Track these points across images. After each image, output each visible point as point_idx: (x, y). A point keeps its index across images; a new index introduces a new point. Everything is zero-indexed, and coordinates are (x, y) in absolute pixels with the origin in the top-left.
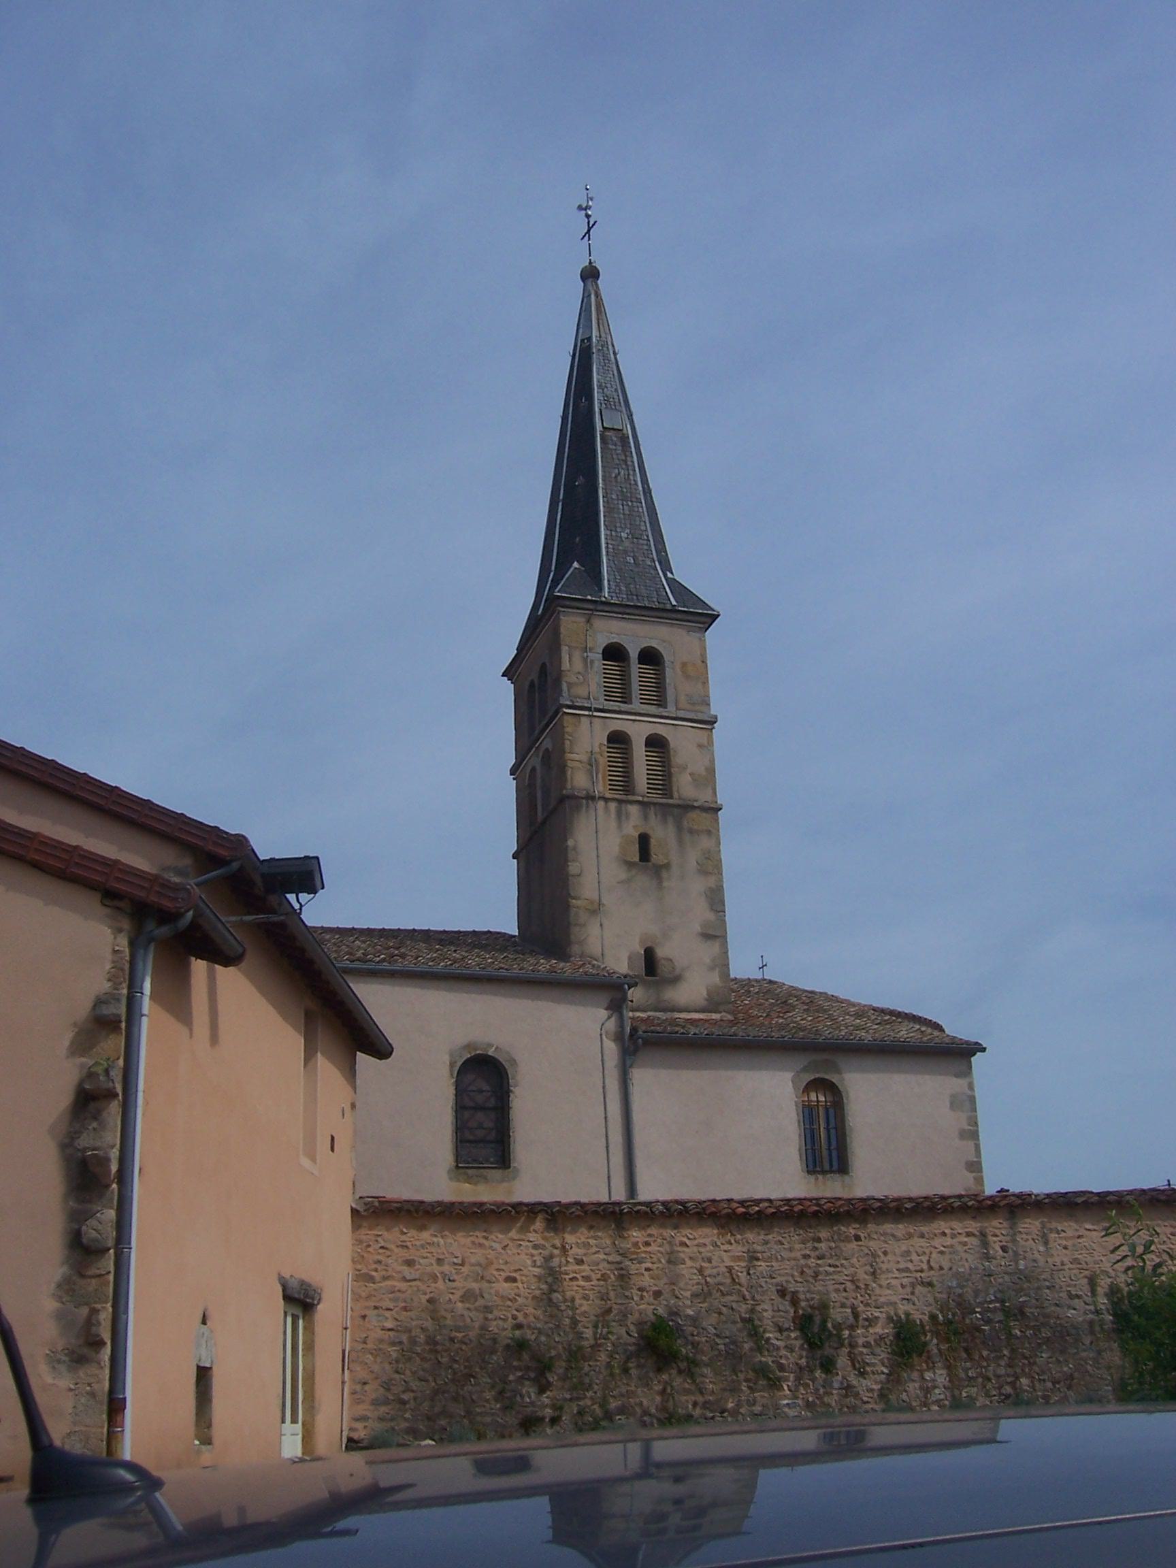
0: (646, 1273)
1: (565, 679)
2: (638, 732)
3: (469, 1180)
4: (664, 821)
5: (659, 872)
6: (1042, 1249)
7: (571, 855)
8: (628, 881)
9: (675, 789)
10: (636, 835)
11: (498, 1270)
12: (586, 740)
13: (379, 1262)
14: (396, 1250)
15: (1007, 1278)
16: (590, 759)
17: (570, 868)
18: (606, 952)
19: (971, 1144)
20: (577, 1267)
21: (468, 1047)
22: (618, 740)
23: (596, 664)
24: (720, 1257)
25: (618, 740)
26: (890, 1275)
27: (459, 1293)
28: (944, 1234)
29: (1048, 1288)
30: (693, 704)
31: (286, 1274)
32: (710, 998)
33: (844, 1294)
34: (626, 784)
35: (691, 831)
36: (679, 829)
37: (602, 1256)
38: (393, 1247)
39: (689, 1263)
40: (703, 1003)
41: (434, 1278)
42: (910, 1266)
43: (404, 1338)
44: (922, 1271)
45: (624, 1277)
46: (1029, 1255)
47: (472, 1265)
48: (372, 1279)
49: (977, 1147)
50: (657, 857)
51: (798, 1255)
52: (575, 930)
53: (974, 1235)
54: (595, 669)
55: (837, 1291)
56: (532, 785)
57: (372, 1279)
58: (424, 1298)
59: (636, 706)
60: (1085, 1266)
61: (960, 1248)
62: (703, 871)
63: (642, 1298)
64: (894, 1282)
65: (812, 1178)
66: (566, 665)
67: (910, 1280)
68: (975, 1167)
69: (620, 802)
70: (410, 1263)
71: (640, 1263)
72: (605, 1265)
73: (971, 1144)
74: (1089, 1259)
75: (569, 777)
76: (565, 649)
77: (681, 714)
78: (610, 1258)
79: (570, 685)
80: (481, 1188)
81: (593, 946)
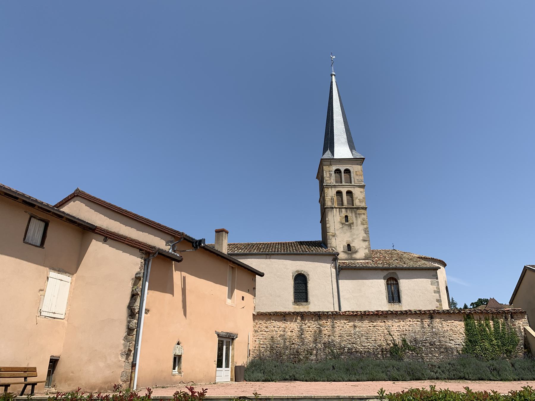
2: (344, 190)
3: (297, 305)
4: (352, 212)
5: (350, 225)
7: (327, 222)
8: (342, 227)
12: (331, 193)
15: (429, 334)
21: (297, 271)
22: (339, 193)
25: (339, 193)
28: (410, 321)
31: (220, 331)
32: (365, 257)
35: (359, 214)
36: (356, 214)
41: (273, 331)
43: (265, 346)
45: (320, 331)
48: (258, 332)
49: (440, 296)
50: (350, 221)
51: (368, 326)
52: (328, 241)
57: (258, 332)
66: (325, 176)
69: (340, 208)
70: (267, 327)
74: (456, 329)
76: (324, 172)
79: (326, 180)
81: (334, 245)
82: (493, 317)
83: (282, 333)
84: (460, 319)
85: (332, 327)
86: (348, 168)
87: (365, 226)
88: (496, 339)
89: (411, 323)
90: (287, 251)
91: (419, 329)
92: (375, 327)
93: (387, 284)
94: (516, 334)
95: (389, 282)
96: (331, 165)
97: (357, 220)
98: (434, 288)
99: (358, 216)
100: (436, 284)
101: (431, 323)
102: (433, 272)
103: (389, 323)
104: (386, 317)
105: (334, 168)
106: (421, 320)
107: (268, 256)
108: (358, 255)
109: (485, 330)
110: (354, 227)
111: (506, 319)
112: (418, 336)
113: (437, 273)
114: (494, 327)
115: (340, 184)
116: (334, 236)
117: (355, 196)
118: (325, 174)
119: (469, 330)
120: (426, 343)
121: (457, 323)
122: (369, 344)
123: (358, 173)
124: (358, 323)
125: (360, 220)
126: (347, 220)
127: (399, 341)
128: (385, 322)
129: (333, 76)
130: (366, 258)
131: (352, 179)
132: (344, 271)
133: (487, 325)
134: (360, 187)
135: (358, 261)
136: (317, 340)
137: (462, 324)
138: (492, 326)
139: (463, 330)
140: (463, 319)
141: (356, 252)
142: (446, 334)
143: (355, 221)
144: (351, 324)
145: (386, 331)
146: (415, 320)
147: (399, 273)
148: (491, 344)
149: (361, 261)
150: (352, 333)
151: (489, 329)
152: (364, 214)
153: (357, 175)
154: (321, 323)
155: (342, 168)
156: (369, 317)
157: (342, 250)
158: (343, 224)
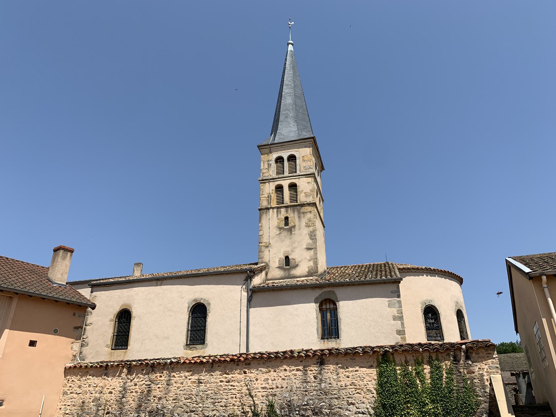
0: (158, 389)
2: (285, 184)
3: (190, 349)
4: (294, 212)
5: (290, 230)
8: (280, 233)
9: (298, 199)
10: (283, 218)
13: (70, 387)
14: (77, 382)
15: (315, 393)
19: (399, 322)
22: (279, 188)
26: (257, 390)
28: (285, 370)
29: (336, 398)
32: (309, 272)
33: (235, 399)
34: (281, 200)
35: (303, 213)
36: (299, 213)
37: (144, 382)
39: (175, 385)
40: (307, 274)
41: (86, 393)
42: (267, 386)
44: (273, 389)
46: (328, 380)
49: (403, 324)
53: (300, 370)
58: (82, 400)
60: (358, 387)
61: (292, 377)
62: (308, 226)
67: (266, 393)
68: (401, 332)
69: (278, 208)
70: (80, 387)
72: (144, 386)
74: (361, 383)
77: (302, 174)
78: (146, 383)
79: (263, 173)
80: (194, 352)
82: (430, 357)
83: (97, 395)
84: (370, 364)
85: (168, 385)
86: (293, 153)
87: (311, 229)
88: (433, 402)
89: (288, 373)
90: (386, 276)
91: (297, 383)
92: (228, 382)
93: (321, 310)
94: (474, 391)
95: (324, 307)
96: (271, 152)
97: (300, 221)
98: (394, 311)
99: (302, 215)
100: (397, 305)
101: (320, 374)
102: (393, 287)
103: (252, 374)
104: (249, 364)
105: (275, 155)
106: (304, 367)
107: (159, 282)
108: (297, 272)
109: (412, 384)
110: (296, 232)
111: (456, 360)
112: (295, 398)
113: (398, 287)
114: (431, 378)
115: (282, 176)
116: (267, 247)
117: (299, 189)
118: (262, 165)
119: (383, 386)
120: (306, 410)
121: (364, 371)
122: (215, 412)
123: (305, 158)
124: (205, 376)
125: (304, 221)
126: (287, 224)
127: (262, 407)
128: (245, 373)
129: (290, 45)
130: (310, 274)
131: (298, 167)
132: (258, 296)
133: (418, 373)
134: (307, 176)
135: (298, 279)
136: (140, 406)
137: (373, 372)
138: (428, 376)
139: (372, 385)
140: (375, 364)
141: (297, 266)
142: (343, 393)
143: (297, 224)
144: (195, 377)
145: (245, 390)
146: (293, 368)
147: (339, 292)
148: (422, 412)
149: (302, 279)
150: (193, 393)
151: (420, 381)
152: (310, 212)
153: (304, 161)
154: (153, 376)
155: (285, 155)
156: (223, 365)
157: (277, 265)
158: (280, 229)
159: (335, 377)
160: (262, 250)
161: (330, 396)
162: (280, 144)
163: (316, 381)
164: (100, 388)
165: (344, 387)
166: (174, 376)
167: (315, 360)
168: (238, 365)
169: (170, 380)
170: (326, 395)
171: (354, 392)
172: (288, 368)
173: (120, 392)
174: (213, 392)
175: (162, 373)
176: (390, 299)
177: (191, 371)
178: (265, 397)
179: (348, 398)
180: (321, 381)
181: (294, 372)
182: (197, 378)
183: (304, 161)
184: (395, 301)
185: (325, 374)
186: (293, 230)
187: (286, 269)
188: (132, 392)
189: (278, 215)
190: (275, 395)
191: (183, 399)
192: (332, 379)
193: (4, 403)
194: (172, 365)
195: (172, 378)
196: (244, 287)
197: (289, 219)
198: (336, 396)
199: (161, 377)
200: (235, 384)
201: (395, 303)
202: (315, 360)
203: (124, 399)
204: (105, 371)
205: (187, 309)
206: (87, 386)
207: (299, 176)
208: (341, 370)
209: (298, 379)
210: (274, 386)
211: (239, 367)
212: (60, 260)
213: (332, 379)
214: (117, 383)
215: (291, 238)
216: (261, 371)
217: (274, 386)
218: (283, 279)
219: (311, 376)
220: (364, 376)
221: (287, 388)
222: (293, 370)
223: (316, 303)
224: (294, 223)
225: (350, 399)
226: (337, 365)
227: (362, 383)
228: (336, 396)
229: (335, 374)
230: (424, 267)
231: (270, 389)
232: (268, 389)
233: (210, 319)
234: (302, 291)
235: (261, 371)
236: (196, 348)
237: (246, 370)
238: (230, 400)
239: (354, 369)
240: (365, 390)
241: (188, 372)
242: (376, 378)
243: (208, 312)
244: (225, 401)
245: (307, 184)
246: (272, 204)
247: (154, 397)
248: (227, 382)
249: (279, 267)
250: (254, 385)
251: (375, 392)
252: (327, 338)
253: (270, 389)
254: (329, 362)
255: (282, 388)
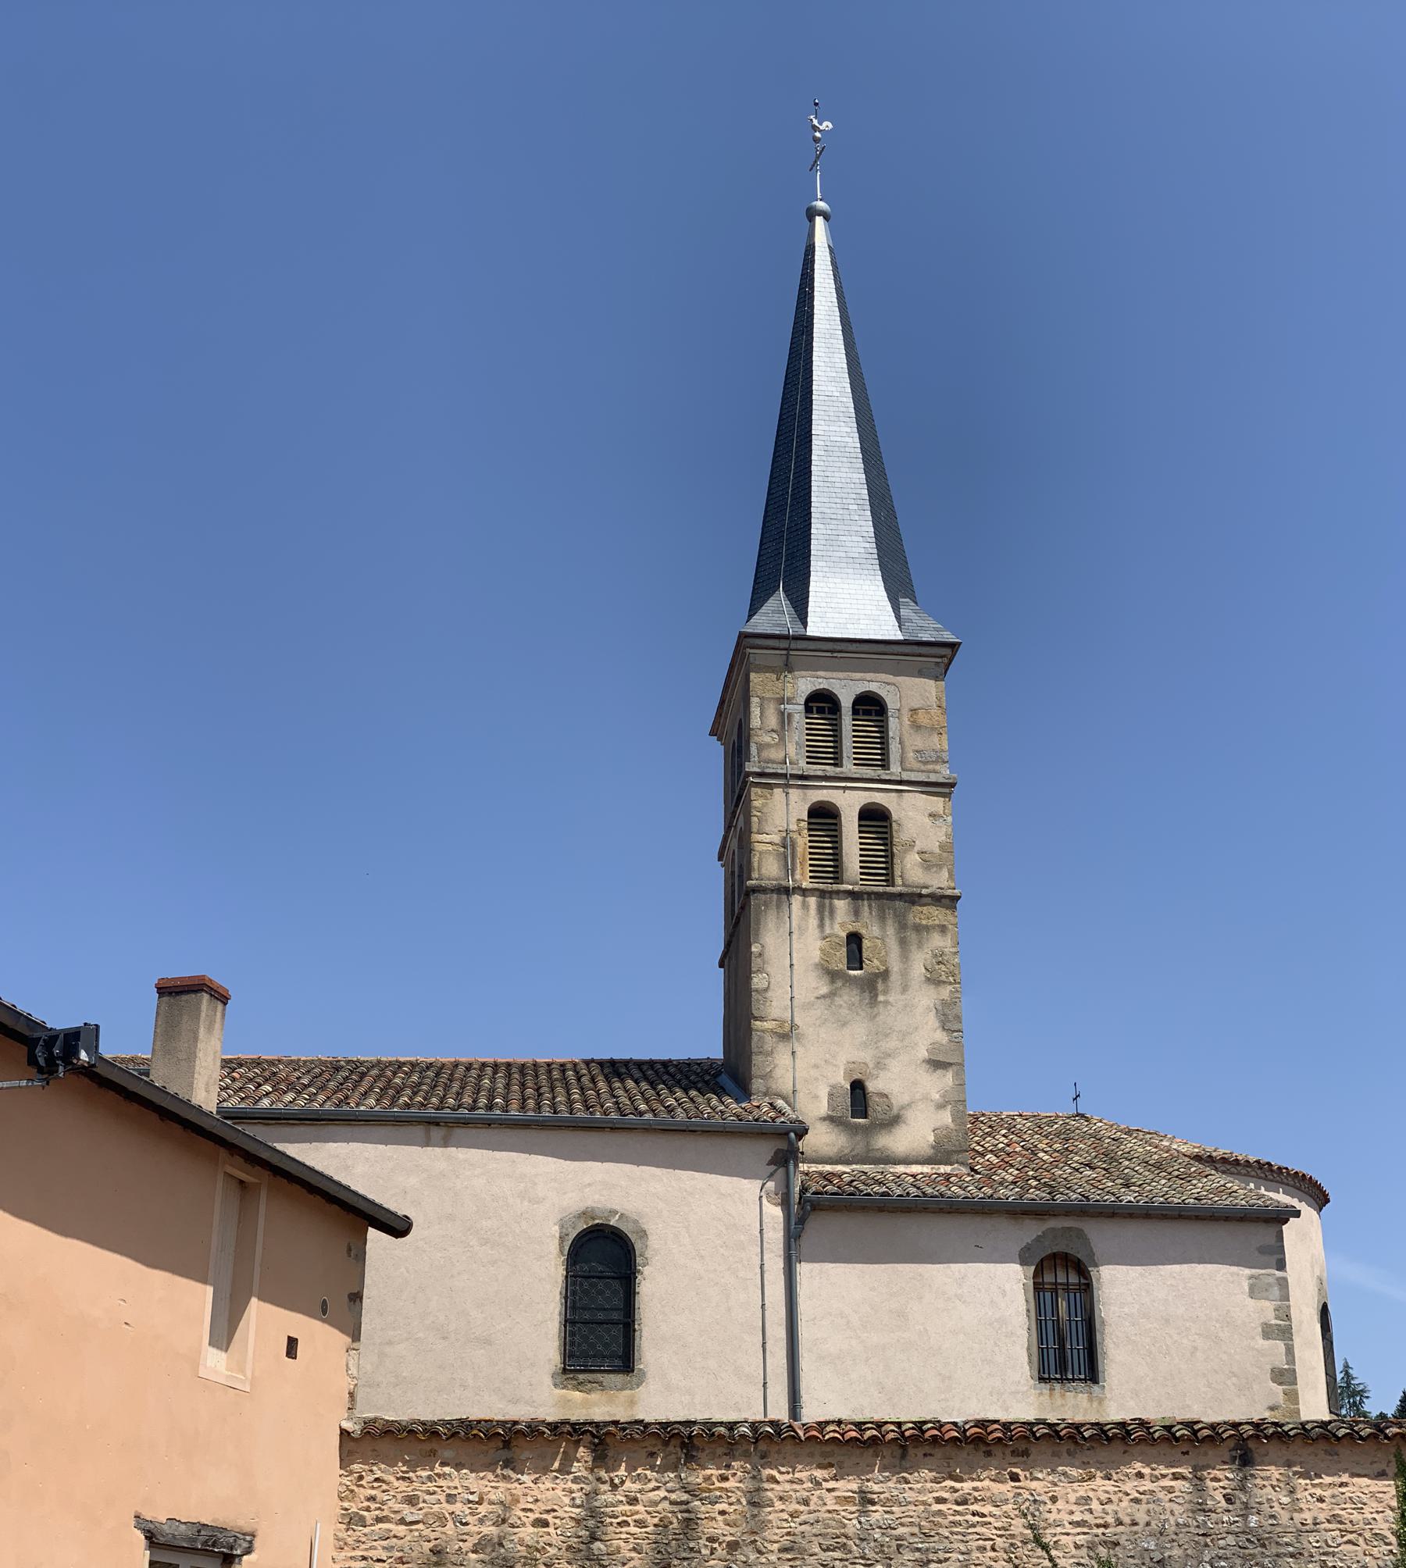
0: (720, 1518)
1: (754, 739)
2: (849, 803)
3: (579, 1386)
4: (882, 919)
5: (872, 986)
6: (1285, 1500)
7: (756, 963)
8: (831, 995)
9: (897, 873)
10: (844, 935)
11: (524, 1510)
12: (781, 814)
13: (372, 1499)
14: (396, 1484)
15: (1231, 1540)
16: (785, 838)
17: (755, 980)
18: (798, 1087)
19: (1280, 1346)
20: (628, 1508)
21: (584, 1214)
22: (823, 816)
23: (797, 717)
24: (820, 1498)
25: (823, 816)
27: (472, 1541)
28: (1140, 1475)
29: (1292, 1556)
30: (926, 763)
32: (937, 1146)
33: (993, 1554)
35: (918, 928)
36: (902, 926)
37: (662, 1493)
38: (392, 1479)
39: (779, 1505)
41: (442, 1520)
42: (1087, 1517)
44: (1106, 1526)
45: (690, 1523)
47: (491, 1503)
49: (1290, 1351)
51: (929, 1498)
52: (757, 1060)
54: (795, 725)
55: (982, 1549)
56: (733, 873)
58: (428, 1546)
59: (848, 767)
60: (1349, 1526)
61: (1161, 1495)
63: (713, 1551)
64: (1064, 1539)
65: (1045, 1387)
66: (755, 722)
70: (411, 1500)
71: (713, 1503)
72: (666, 1505)
73: (1280, 1346)
74: (1356, 1516)
75: (756, 865)
76: (755, 701)
77: (906, 776)
78: (673, 1496)
79: (761, 747)
83: (489, 1530)
85: (753, 1504)
86: (873, 687)
89: (1147, 1485)
93: (1038, 1288)
95: (1049, 1278)
96: (788, 667)
97: (905, 956)
98: (1266, 1310)
99: (912, 936)
100: (1276, 1291)
101: (1243, 1489)
102: (1262, 1234)
103: (1039, 1483)
105: (804, 684)
106: (1195, 1469)
107: (437, 1133)
108: (899, 1141)
112: (1176, 1552)
113: (1280, 1237)
115: (831, 770)
116: (785, 1037)
117: (901, 836)
118: (755, 711)
123: (922, 718)
124: (881, 1484)
126: (856, 958)
128: (1015, 1478)
135: (900, 1169)
137: (1388, 1489)
139: (1387, 1524)
140: (1392, 1469)
143: (895, 966)
144: (848, 1486)
145: (1018, 1526)
147: (1099, 1235)
149: (916, 1169)
150: (850, 1531)
152: (943, 929)
153: (917, 727)
154: (696, 1478)
155: (846, 688)
156: (938, 1452)
157: (823, 1109)
158: (833, 975)
159: (1285, 1500)
160: (768, 1047)
161: (1274, 1550)
162: (830, 646)
163: (1230, 1507)
164: (499, 1509)
165: (1310, 1527)
166: (772, 1479)
167: (1224, 1451)
168: (988, 1454)
169: (758, 1490)
170: (1264, 1546)
171: (1340, 1540)
172: (1146, 1471)
173: (578, 1521)
174: (916, 1530)
175: (728, 1467)
176: (1254, 1271)
177: (831, 1465)
178: (1084, 1551)
179: (1324, 1554)
180: (1246, 1508)
181: (1167, 1483)
182: (855, 1486)
183: (917, 727)
184: (1271, 1280)
185: (1255, 1490)
186: (880, 986)
187: (857, 1127)
188: (626, 1523)
189: (822, 920)
190: (1117, 1544)
191: (817, 1550)
192: (1275, 1504)
193: (257, 1543)
194: (762, 1446)
195: (766, 1486)
196: (771, 1185)
197: (866, 943)
198: (1291, 1549)
199: (724, 1478)
200: (987, 1509)
201: (1269, 1285)
202: (1224, 1451)
203: (598, 1544)
204: (505, 1454)
205: (557, 1241)
206: (443, 1498)
207: (900, 782)
208: (1301, 1481)
209: (1180, 1500)
210: (1110, 1520)
211: (995, 1462)
212: (202, 1031)
213: (1275, 1504)
214: (559, 1493)
215: (873, 1018)
216: (1065, 1474)
217: (1110, 1520)
218: (847, 1163)
219: (1216, 1496)
220: (1364, 1498)
221: (1148, 1524)
222: (1164, 1476)
223: (1023, 1262)
224: (884, 962)
225: (1331, 1558)
226: (1289, 1466)
227: (1360, 1517)
228: (1291, 1549)
229: (1285, 1493)
230: (1252, 1159)
231: (1098, 1526)
232: (1090, 1527)
233: (651, 1287)
234: (978, 1219)
235: (1065, 1474)
236: (601, 1384)
237: (1017, 1470)
238: (975, 1554)
239: (1336, 1480)
240: (1368, 1535)
241: (820, 1467)
242: (1394, 1503)
243: (639, 1260)
244: (961, 1558)
245: (927, 820)
246: (798, 877)
247: (712, 1540)
248: (958, 1503)
249: (830, 1119)
250: (1048, 1515)
251: (1393, 1539)
252: (1061, 1380)
253: (1098, 1526)
254: (1266, 1459)
255: (1134, 1524)
